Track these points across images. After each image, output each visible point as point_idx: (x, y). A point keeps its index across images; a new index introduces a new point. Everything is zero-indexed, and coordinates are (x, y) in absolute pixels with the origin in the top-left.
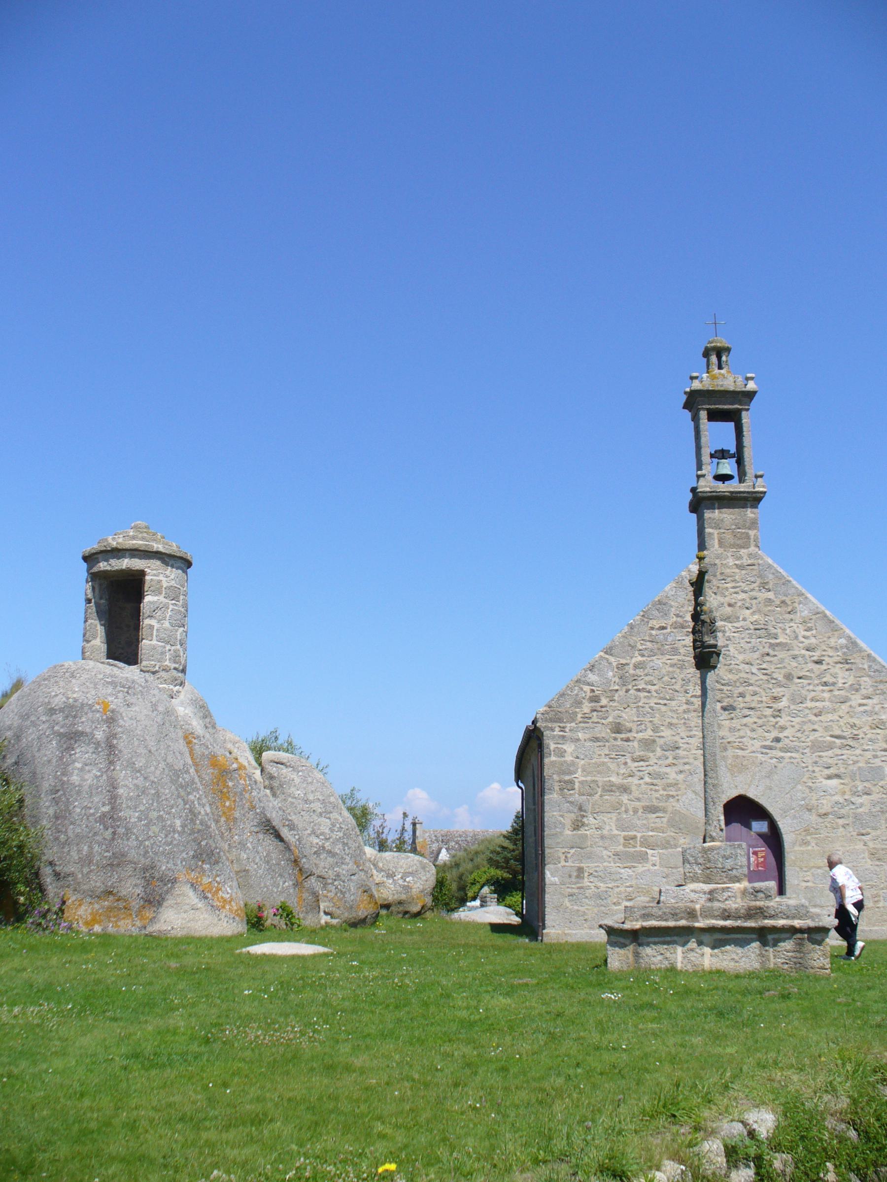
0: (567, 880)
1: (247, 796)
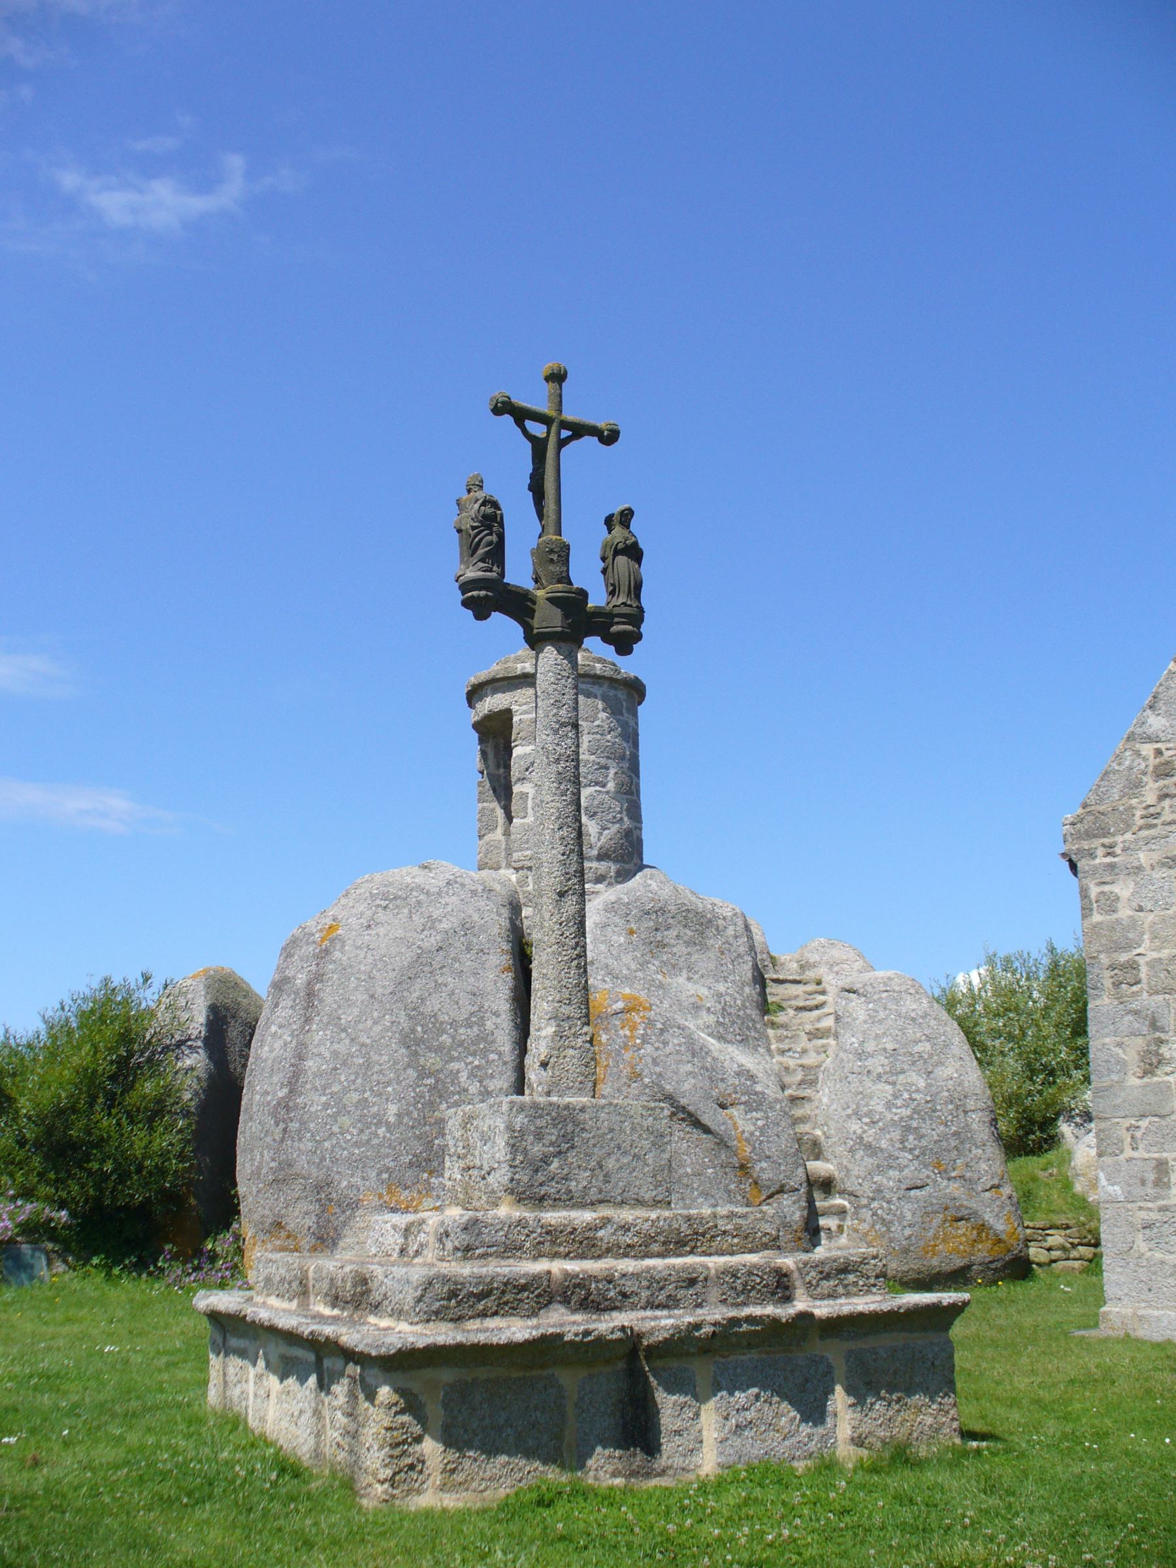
0: (1138, 1191)
1: (627, 1056)
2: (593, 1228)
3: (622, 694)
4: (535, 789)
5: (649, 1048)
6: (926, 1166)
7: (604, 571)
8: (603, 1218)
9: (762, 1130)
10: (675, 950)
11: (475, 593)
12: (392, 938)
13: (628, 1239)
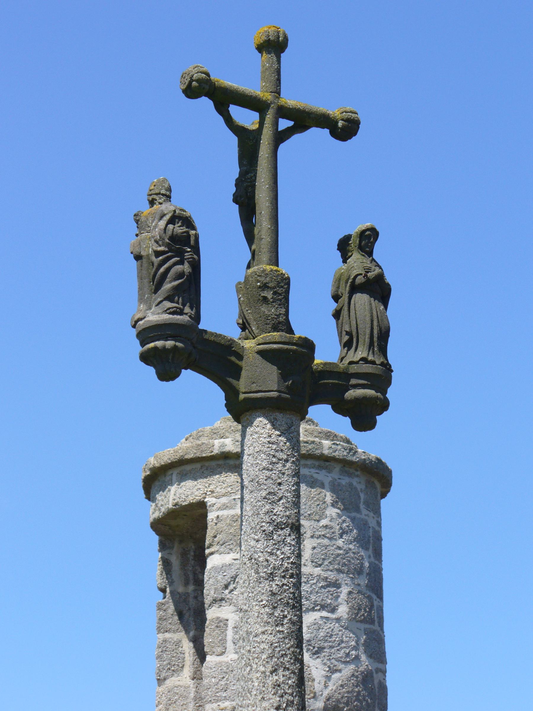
3: (358, 483)
4: (238, 615)
7: (337, 315)
11: (159, 344)
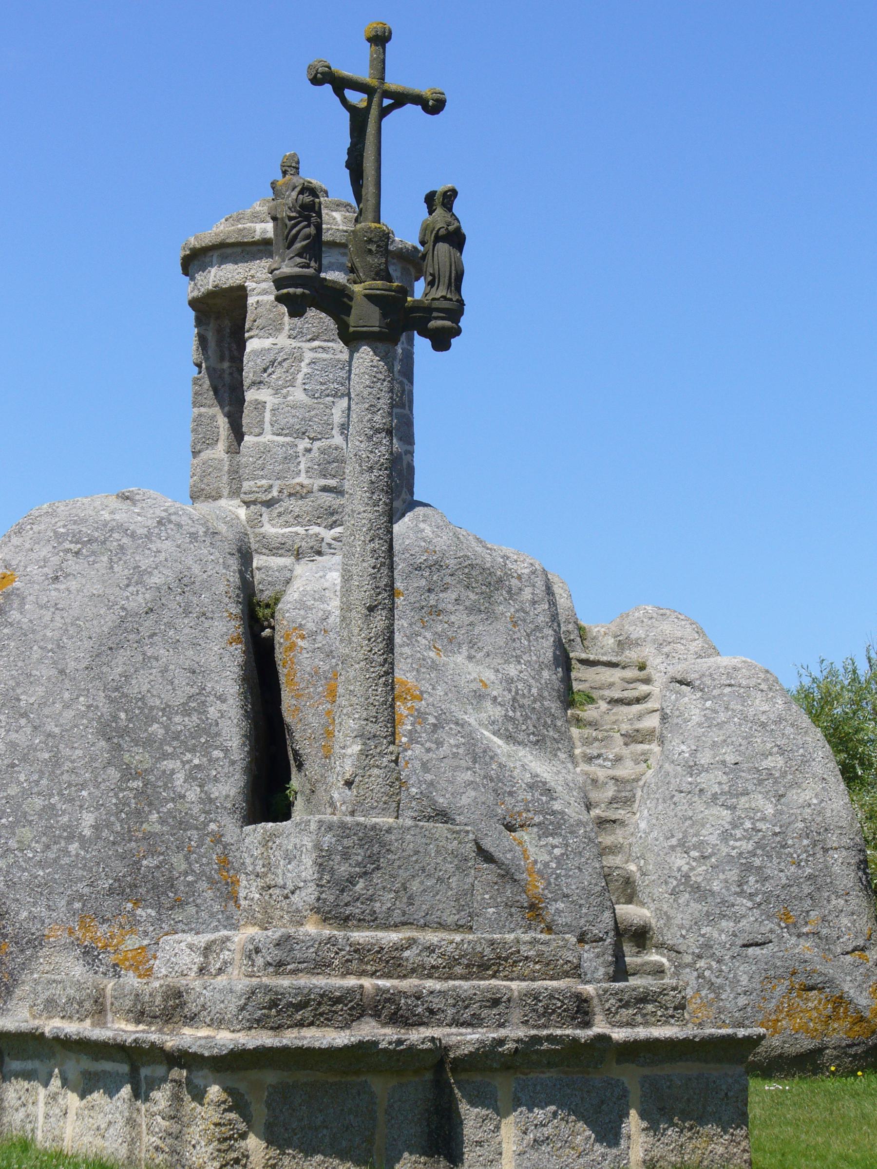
2: (399, 948)
5: (418, 749)
6: (769, 917)
8: (409, 939)
9: (558, 860)
10: (453, 618)
11: (291, 290)
12: (86, 594)
13: (432, 960)
